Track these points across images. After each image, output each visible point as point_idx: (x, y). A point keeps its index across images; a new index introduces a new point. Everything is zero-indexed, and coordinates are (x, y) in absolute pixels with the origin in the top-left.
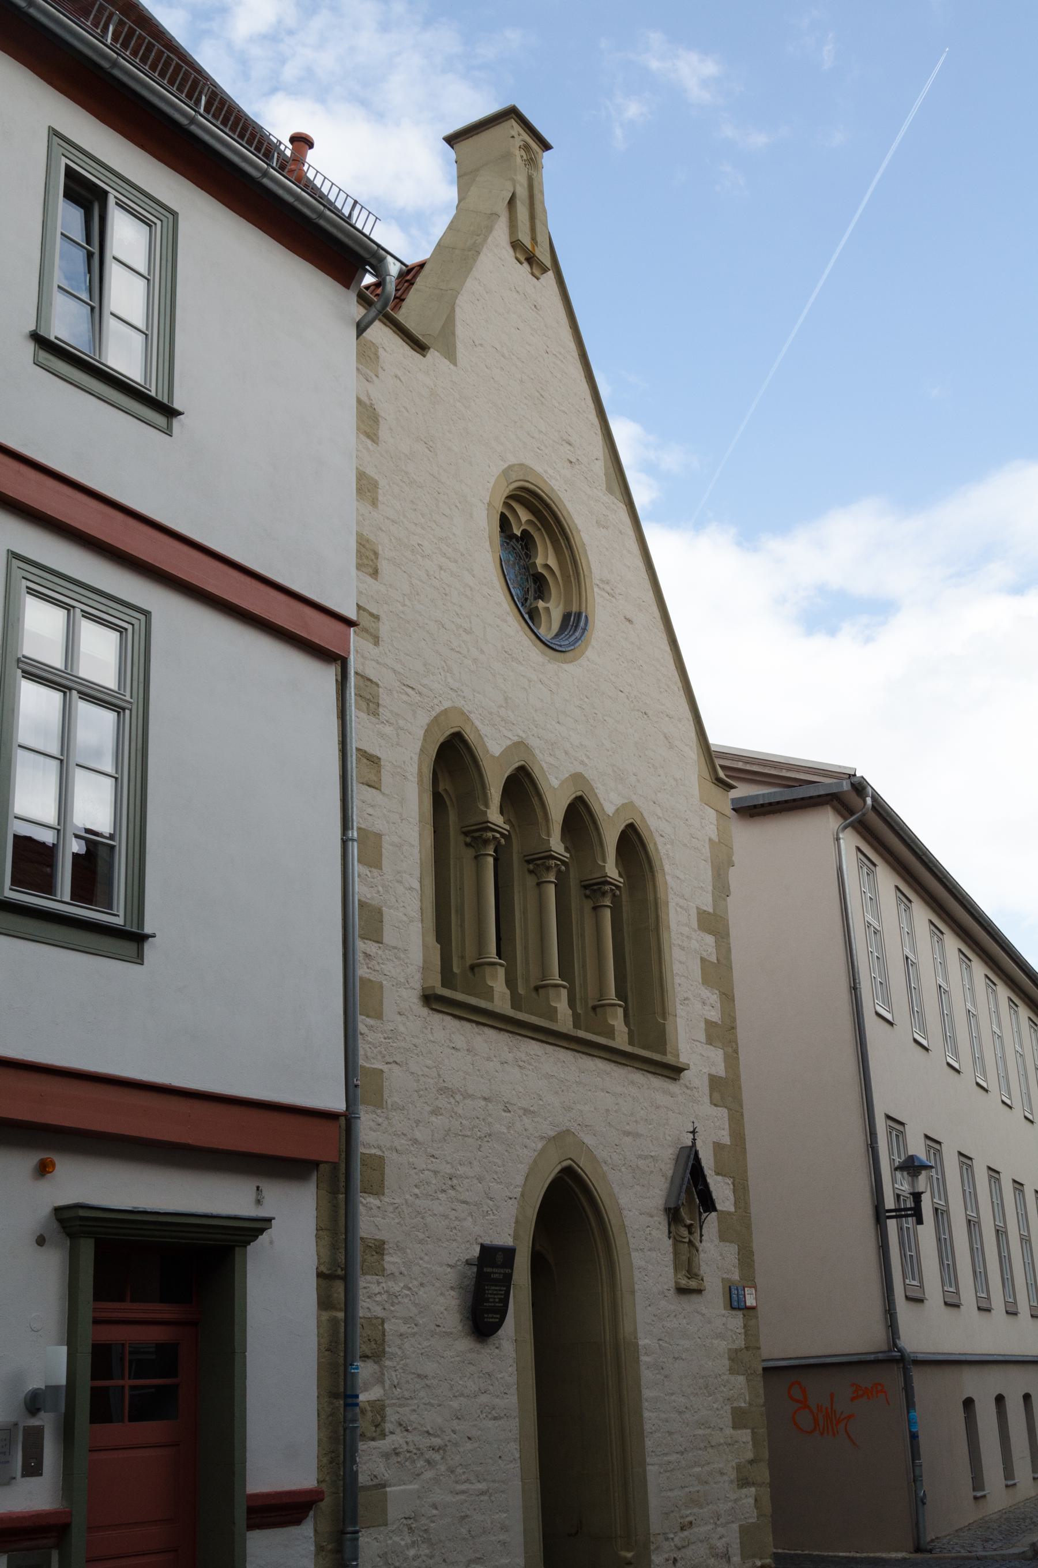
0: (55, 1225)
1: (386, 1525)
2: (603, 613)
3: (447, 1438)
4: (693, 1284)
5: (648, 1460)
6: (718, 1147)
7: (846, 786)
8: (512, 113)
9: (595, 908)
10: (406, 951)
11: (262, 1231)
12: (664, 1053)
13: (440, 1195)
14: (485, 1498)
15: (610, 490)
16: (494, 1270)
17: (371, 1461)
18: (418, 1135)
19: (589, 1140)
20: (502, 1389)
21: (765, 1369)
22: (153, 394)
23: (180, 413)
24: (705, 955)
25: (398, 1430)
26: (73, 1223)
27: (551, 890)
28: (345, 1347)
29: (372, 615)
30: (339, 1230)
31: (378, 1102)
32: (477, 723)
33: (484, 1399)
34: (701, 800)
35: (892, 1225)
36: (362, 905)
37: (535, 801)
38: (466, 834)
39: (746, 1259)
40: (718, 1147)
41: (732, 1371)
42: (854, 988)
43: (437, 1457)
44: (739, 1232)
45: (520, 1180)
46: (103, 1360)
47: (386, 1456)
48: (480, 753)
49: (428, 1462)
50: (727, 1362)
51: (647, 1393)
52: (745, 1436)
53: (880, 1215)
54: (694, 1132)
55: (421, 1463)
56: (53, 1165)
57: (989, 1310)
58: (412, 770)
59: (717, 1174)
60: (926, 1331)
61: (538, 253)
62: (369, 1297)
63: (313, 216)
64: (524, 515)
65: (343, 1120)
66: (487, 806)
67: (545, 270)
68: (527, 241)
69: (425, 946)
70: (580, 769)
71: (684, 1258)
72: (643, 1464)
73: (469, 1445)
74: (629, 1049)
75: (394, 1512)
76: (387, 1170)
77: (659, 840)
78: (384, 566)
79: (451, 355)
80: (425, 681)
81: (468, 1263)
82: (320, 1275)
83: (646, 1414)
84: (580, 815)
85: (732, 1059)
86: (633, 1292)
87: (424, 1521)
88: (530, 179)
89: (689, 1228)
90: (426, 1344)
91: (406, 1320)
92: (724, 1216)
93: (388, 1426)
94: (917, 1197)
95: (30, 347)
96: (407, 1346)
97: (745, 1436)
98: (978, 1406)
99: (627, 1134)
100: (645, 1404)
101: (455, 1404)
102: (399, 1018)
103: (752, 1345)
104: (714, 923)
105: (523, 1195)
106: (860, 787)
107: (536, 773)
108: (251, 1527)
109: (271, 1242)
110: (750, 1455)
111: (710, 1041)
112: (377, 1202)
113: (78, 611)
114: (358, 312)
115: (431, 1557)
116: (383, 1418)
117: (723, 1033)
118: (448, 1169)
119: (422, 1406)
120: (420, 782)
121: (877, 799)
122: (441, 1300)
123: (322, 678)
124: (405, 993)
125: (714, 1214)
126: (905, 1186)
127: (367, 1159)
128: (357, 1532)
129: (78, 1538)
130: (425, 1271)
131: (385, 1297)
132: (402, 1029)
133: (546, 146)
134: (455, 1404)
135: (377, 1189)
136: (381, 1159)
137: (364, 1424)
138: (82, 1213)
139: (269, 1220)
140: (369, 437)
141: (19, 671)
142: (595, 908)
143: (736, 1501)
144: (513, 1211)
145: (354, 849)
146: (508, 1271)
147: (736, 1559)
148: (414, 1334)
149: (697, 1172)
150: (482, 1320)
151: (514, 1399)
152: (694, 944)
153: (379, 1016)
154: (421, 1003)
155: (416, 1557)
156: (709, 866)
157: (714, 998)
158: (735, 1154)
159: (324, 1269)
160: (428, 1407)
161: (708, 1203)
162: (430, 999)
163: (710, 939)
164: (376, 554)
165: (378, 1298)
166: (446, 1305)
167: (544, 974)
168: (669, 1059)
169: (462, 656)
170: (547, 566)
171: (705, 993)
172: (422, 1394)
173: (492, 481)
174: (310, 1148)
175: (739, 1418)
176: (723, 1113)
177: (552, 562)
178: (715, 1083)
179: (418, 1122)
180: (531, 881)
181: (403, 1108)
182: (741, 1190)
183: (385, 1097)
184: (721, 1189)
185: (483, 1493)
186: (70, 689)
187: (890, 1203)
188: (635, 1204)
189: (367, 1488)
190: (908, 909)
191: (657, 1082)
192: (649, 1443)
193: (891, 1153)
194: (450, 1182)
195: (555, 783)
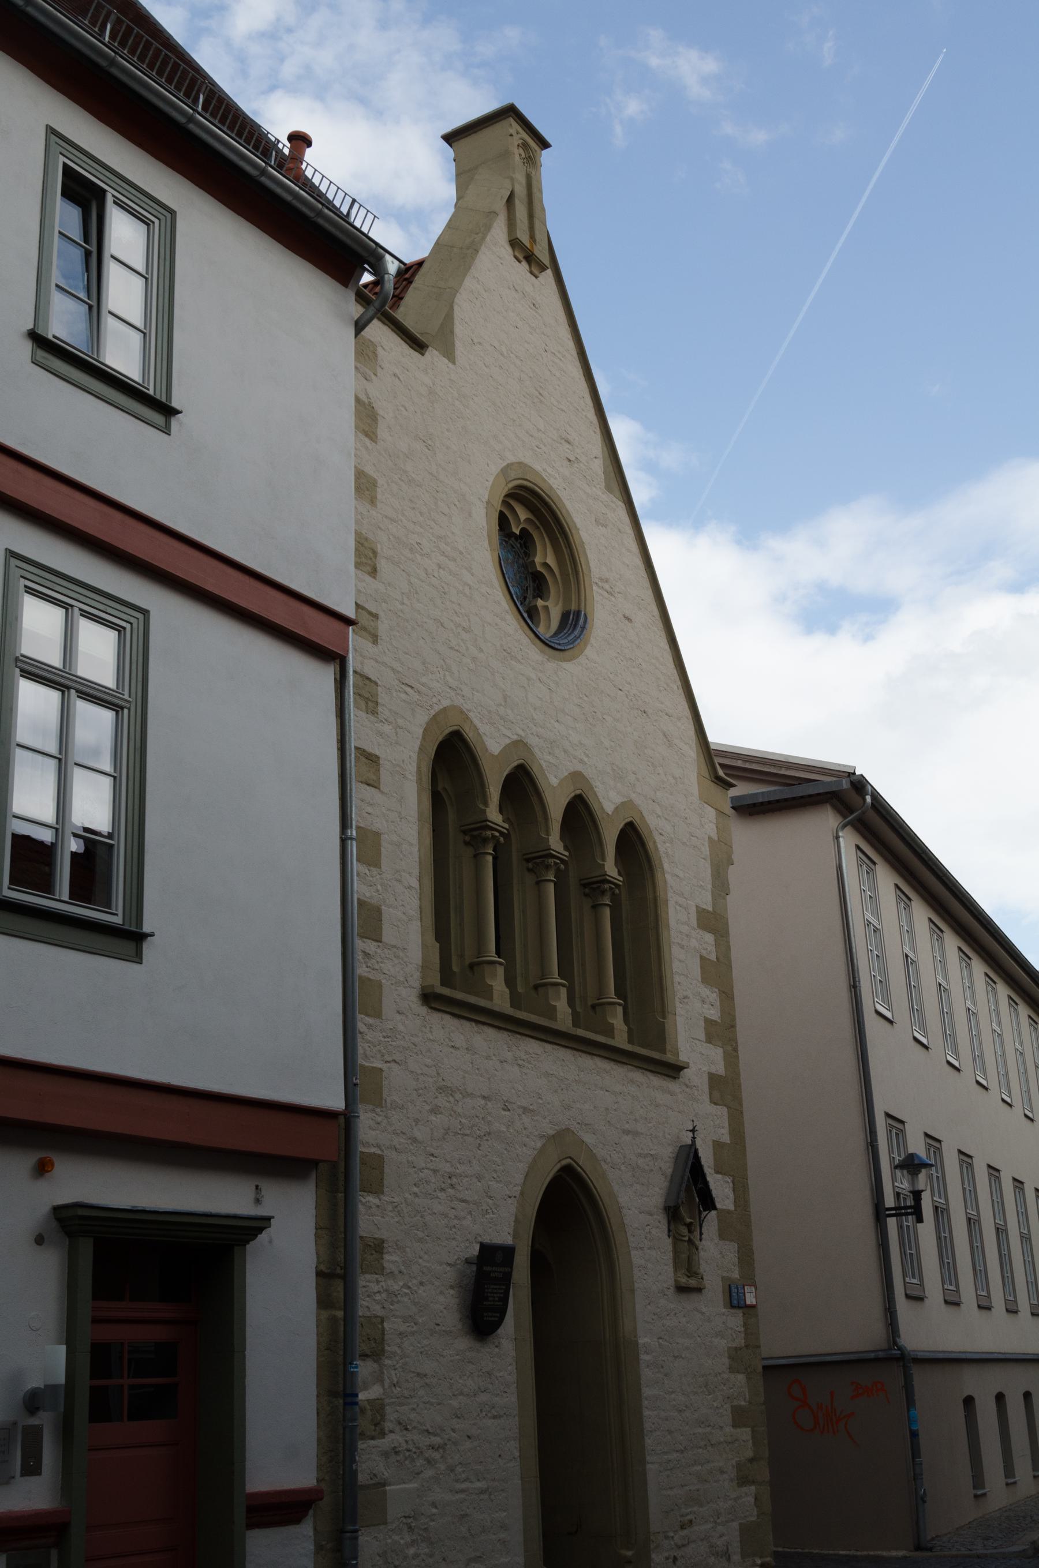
1: (385, 1523)
4: (693, 1282)
6: (718, 1145)
7: (845, 784)
8: (510, 112)
9: (595, 907)
10: (405, 949)
11: (261, 1230)
15: (608, 488)
17: (371, 1459)
18: (418, 1135)
19: (588, 1139)
21: (765, 1368)
22: (151, 392)
23: (178, 412)
24: (704, 953)
26: (72, 1223)
29: (370, 613)
31: (377, 1100)
32: (476, 722)
33: (483, 1397)
35: (892, 1223)
38: (465, 832)
39: (746, 1257)
40: (718, 1145)
41: (732, 1370)
42: (854, 987)
43: (436, 1455)
44: (739, 1230)
45: (519, 1178)
47: (385, 1455)
48: (479, 752)
49: (429, 1461)
50: (726, 1361)
53: (880, 1213)
54: (693, 1131)
55: (420, 1462)
57: (957, 1304)
59: (717, 1172)
60: (927, 1329)
61: (536, 252)
63: (311, 214)
64: (523, 514)
65: (342, 1120)
67: (543, 268)
68: (525, 240)
69: (424, 946)
70: (579, 767)
71: (684, 1256)
76: (387, 1170)
77: (658, 839)
78: (382, 564)
79: (449, 354)
80: (424, 680)
81: (468, 1261)
83: (646, 1413)
85: (732, 1058)
88: (529, 178)
89: (689, 1226)
90: (425, 1342)
92: (723, 1215)
93: (388, 1425)
94: (917, 1195)
95: (28, 346)
99: (627, 1132)
100: (645, 1403)
101: (455, 1403)
102: (398, 1017)
103: (752, 1341)
105: (522, 1193)
106: (859, 785)
109: (270, 1242)
110: (749, 1454)
111: (709, 1039)
112: (376, 1201)
114: (356, 310)
115: (431, 1556)
117: (722, 1032)
118: (447, 1168)
121: (876, 796)
122: (441, 1299)
125: (713, 1213)
128: (356, 1531)
131: (384, 1295)
132: (401, 1028)
133: (545, 144)
135: (376, 1188)
137: (364, 1423)
138: (81, 1212)
139: (268, 1219)
140: (367, 435)
141: (17, 670)
142: (595, 907)
145: (353, 847)
147: (736, 1558)
148: (413, 1333)
150: (481, 1318)
151: (514, 1399)
152: (694, 943)
153: (378, 1014)
155: (416, 1556)
156: (708, 866)
158: (734, 1154)
159: (322, 1267)
161: (708, 1202)
162: (428, 998)
163: (709, 938)
164: (375, 553)
165: (378, 1297)
166: (444, 1303)
167: (544, 973)
168: (669, 1057)
170: (546, 565)
171: (705, 991)
173: (491, 479)
174: (308, 1147)
175: (739, 1417)
177: (551, 560)
178: (714, 1080)
179: (417, 1121)
186: (69, 688)
187: (890, 1201)
188: (635, 1202)
191: (656, 1081)
192: (648, 1441)
195: (554, 781)
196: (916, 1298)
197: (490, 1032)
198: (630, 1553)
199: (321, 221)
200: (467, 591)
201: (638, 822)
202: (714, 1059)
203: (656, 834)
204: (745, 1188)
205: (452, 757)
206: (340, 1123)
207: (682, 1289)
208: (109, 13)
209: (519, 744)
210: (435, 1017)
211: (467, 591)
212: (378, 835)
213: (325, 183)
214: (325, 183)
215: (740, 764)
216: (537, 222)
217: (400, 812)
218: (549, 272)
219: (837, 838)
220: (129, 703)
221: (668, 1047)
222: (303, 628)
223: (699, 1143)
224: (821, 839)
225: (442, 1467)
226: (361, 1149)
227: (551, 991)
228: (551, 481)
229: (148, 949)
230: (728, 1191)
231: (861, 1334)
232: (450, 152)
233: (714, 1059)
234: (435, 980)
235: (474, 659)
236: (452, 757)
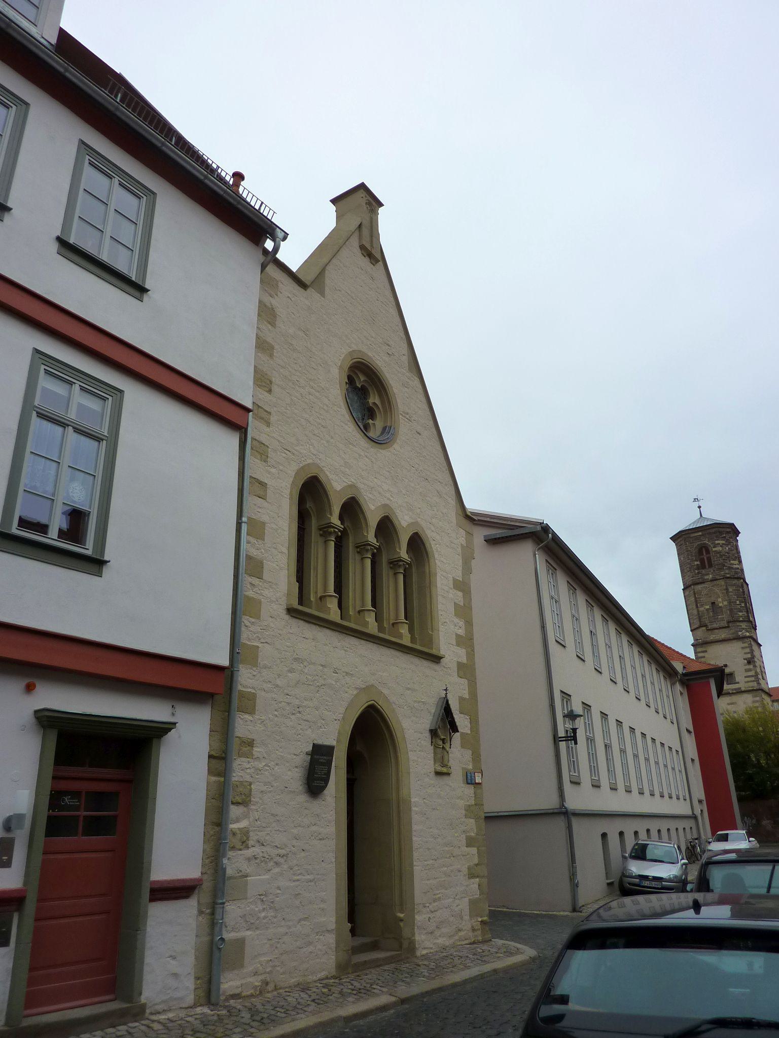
0: (34, 720)
1: (246, 899)
2: (404, 429)
4: (444, 770)
6: (461, 699)
7: (539, 528)
8: (362, 187)
9: (395, 574)
10: (277, 583)
11: (170, 730)
12: (432, 649)
14: (313, 883)
15: (410, 370)
17: (234, 862)
18: (279, 682)
19: (385, 691)
21: (486, 817)
22: (133, 279)
23: (148, 290)
24: (457, 601)
25: (257, 844)
26: (46, 720)
27: (401, 577)
28: (223, 798)
29: (266, 411)
30: (223, 731)
31: (253, 662)
32: (328, 473)
33: (314, 828)
34: (457, 524)
35: (563, 745)
36: (249, 558)
37: (361, 516)
38: (320, 529)
39: (476, 757)
40: (461, 699)
41: (466, 816)
42: (543, 627)
43: (282, 860)
44: (473, 743)
45: (342, 710)
46: (56, 798)
47: (249, 859)
48: (328, 488)
49: (276, 863)
50: (464, 812)
51: (415, 827)
52: (474, 850)
53: (556, 739)
54: (446, 690)
55: (272, 863)
56: (35, 686)
57: (616, 789)
58: (287, 492)
59: (461, 713)
60: (577, 800)
61: (373, 252)
63: (235, 203)
64: (362, 378)
65: (227, 672)
66: (331, 514)
67: (377, 261)
68: (368, 246)
69: (289, 583)
70: (388, 502)
71: (439, 756)
72: (412, 865)
73: (303, 854)
74: (409, 644)
76: (258, 701)
77: (433, 543)
78: (275, 388)
79: (322, 293)
80: (297, 448)
81: (307, 754)
82: (210, 757)
83: (414, 839)
84: (386, 526)
85: (471, 654)
86: (409, 773)
88: (371, 218)
89: (443, 741)
90: (278, 797)
91: (265, 784)
92: (462, 734)
93: (251, 843)
94: (574, 730)
95: (55, 246)
97: (474, 850)
98: (626, 836)
99: (408, 689)
100: (414, 833)
101: (295, 831)
102: (271, 619)
103: (479, 804)
104: (462, 586)
105: (343, 718)
106: (546, 529)
107: (362, 501)
108: (153, 899)
109: (180, 737)
110: (476, 861)
111: (458, 645)
112: (251, 718)
113: (77, 386)
114: (262, 258)
115: (275, 917)
116: (248, 839)
117: (466, 641)
118: (297, 702)
120: (291, 498)
121: (554, 534)
122: (289, 773)
123: (231, 440)
124: (275, 607)
125: (457, 734)
126: (569, 726)
127: (242, 695)
128: (223, 903)
129: (30, 906)
131: (252, 770)
132: (272, 625)
133: (381, 205)
134: (295, 831)
135: (250, 710)
136: (254, 695)
137: (231, 840)
138: (47, 713)
139: (175, 724)
140: (269, 323)
141: (34, 413)
142: (395, 574)
143: (467, 886)
144: (337, 727)
145: (244, 527)
147: (467, 918)
148: (270, 792)
149: (447, 710)
150: (314, 784)
151: (333, 829)
152: (451, 596)
153: (258, 616)
154: (285, 612)
155: (265, 918)
156: (460, 558)
157: (461, 623)
158: (471, 705)
159: (213, 753)
161: (454, 728)
162: (291, 611)
163: (460, 594)
164: (271, 382)
165: (248, 771)
166: (292, 774)
167: (363, 605)
168: (434, 652)
169: (320, 439)
170: (374, 404)
171: (456, 620)
173: (343, 356)
174: (203, 685)
175: (470, 842)
176: (464, 682)
177: (378, 402)
178: (460, 666)
179: (279, 676)
180: (358, 557)
181: (270, 668)
182: (474, 722)
183: (259, 660)
184: (462, 721)
185: (311, 881)
186: (68, 425)
187: (561, 733)
188: (412, 728)
189: (230, 878)
190: (592, 610)
191: (426, 663)
192: (415, 854)
193: (563, 709)
195: (373, 508)
196: (576, 783)
197: (328, 632)
198: (402, 915)
199: (240, 207)
200: (325, 407)
201: (421, 533)
202: (461, 654)
203: (430, 539)
204: (477, 722)
205: (311, 491)
206: (223, 675)
207: (438, 774)
208: (120, 88)
209: (352, 486)
210: (294, 622)
211: (325, 407)
212: (264, 524)
213: (250, 196)
214: (250, 196)
215: (488, 519)
216: (374, 239)
217: (279, 516)
218: (381, 263)
219: (535, 555)
220: (108, 441)
221: (434, 646)
222: (224, 412)
223: (450, 697)
224: (526, 557)
225: (285, 867)
226: (240, 688)
227: (366, 613)
228: (378, 362)
229: (106, 570)
230: (467, 723)
231: (549, 802)
232: (333, 208)
233: (461, 654)
234: (295, 604)
235: (328, 442)
236: (311, 491)
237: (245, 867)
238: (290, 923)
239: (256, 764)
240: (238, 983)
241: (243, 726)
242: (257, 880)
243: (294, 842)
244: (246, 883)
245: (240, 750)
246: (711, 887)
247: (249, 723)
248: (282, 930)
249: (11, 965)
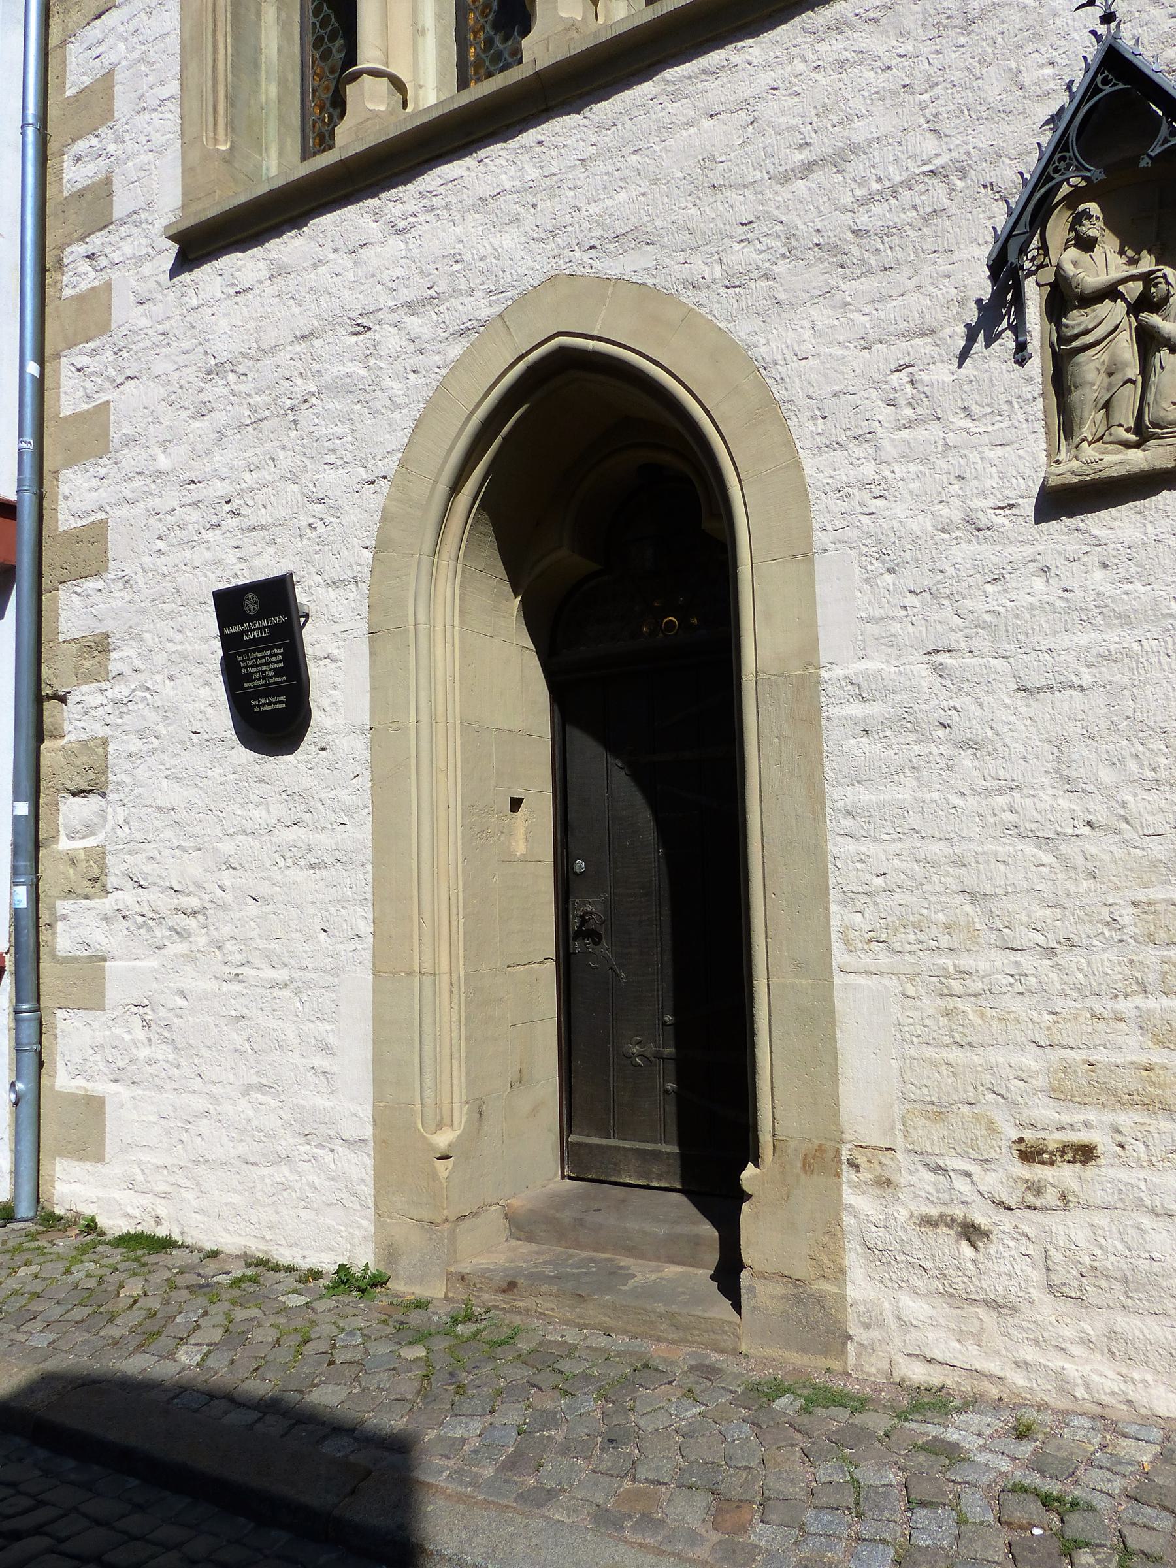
1: (104, 1010)
3: (208, 898)
5: (840, 955)
13: (209, 536)
16: (246, 626)
20: (333, 816)
43: (192, 923)
62: (86, 714)
73: (253, 909)
75: (113, 994)
83: (837, 846)
87: (162, 1012)
93: (111, 881)
96: (138, 771)
101: (226, 847)
112: (100, 584)
116: (104, 870)
119: (166, 852)
130: (173, 657)
134: (226, 847)
146: (226, 631)
155: (149, 1062)
160: (178, 852)
165: (100, 712)
172: (168, 833)
194: (227, 508)
225: (201, 940)
237: (101, 939)
238: (217, 1090)
239: (120, 690)
240: (93, 1193)
241: (74, 611)
242: (129, 971)
243: (227, 878)
244: (103, 969)
245: (77, 668)
246: (102, 176)
247: (96, 597)
248: (197, 1103)
249: (370, 1056)
